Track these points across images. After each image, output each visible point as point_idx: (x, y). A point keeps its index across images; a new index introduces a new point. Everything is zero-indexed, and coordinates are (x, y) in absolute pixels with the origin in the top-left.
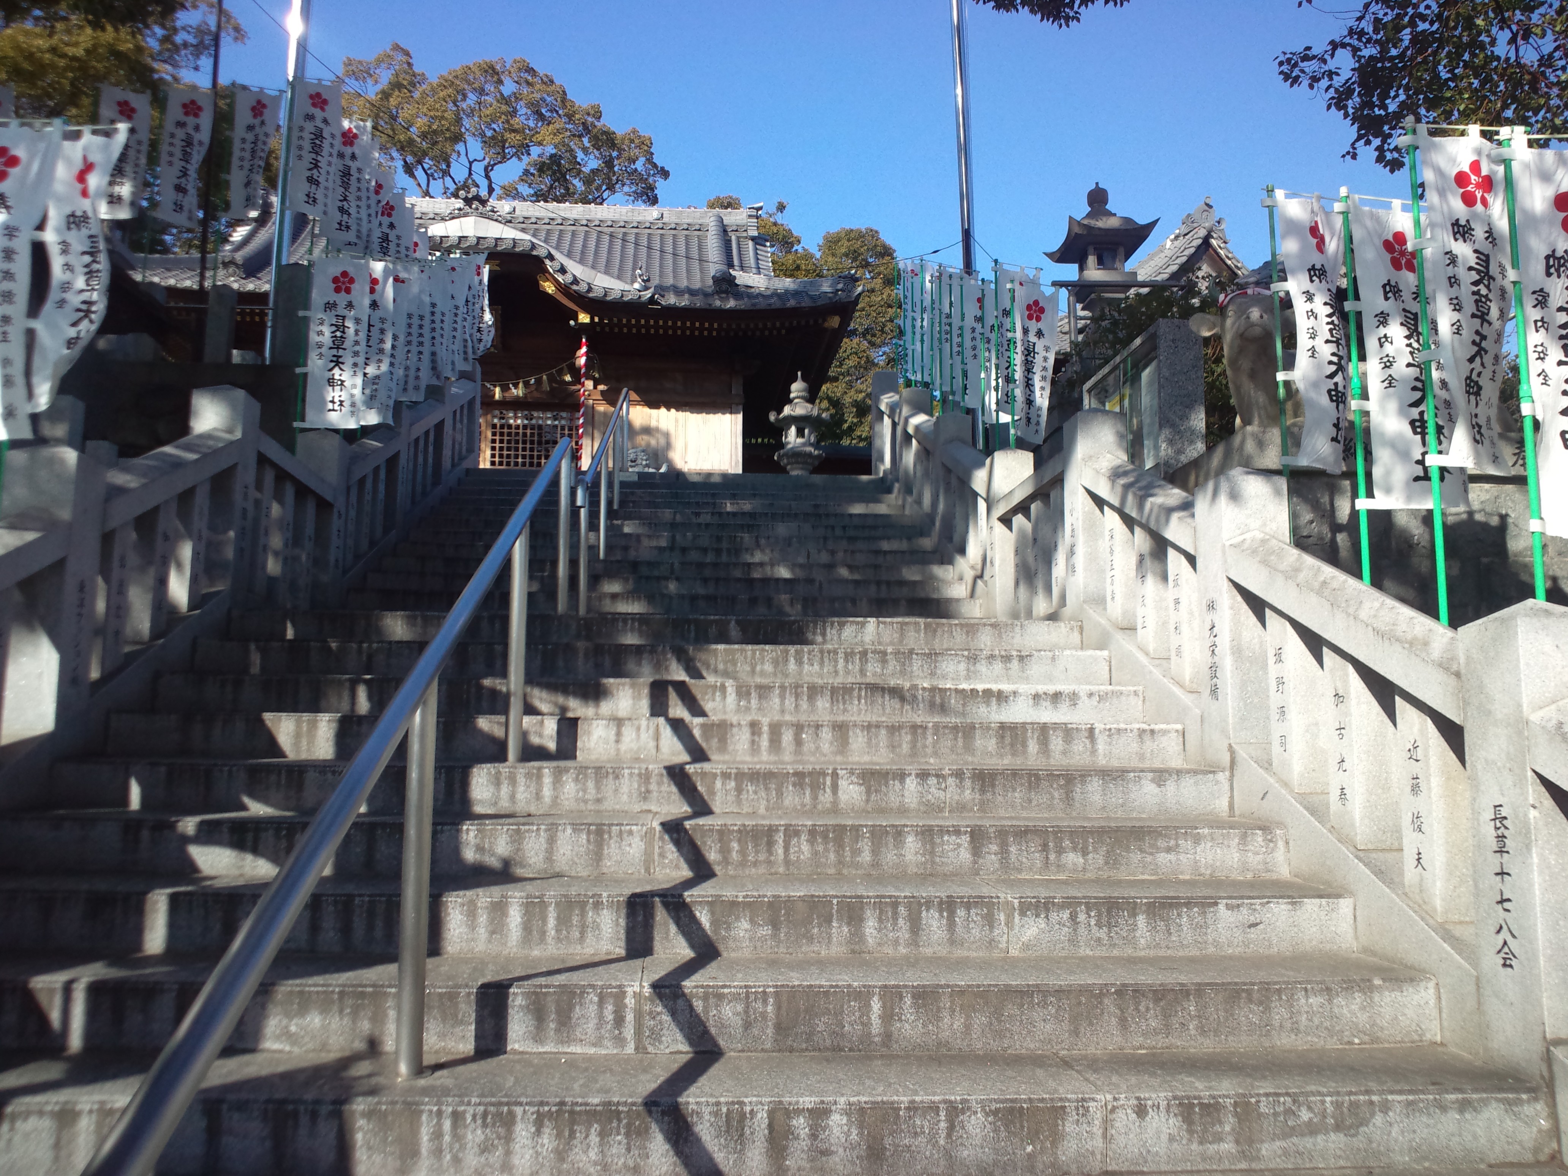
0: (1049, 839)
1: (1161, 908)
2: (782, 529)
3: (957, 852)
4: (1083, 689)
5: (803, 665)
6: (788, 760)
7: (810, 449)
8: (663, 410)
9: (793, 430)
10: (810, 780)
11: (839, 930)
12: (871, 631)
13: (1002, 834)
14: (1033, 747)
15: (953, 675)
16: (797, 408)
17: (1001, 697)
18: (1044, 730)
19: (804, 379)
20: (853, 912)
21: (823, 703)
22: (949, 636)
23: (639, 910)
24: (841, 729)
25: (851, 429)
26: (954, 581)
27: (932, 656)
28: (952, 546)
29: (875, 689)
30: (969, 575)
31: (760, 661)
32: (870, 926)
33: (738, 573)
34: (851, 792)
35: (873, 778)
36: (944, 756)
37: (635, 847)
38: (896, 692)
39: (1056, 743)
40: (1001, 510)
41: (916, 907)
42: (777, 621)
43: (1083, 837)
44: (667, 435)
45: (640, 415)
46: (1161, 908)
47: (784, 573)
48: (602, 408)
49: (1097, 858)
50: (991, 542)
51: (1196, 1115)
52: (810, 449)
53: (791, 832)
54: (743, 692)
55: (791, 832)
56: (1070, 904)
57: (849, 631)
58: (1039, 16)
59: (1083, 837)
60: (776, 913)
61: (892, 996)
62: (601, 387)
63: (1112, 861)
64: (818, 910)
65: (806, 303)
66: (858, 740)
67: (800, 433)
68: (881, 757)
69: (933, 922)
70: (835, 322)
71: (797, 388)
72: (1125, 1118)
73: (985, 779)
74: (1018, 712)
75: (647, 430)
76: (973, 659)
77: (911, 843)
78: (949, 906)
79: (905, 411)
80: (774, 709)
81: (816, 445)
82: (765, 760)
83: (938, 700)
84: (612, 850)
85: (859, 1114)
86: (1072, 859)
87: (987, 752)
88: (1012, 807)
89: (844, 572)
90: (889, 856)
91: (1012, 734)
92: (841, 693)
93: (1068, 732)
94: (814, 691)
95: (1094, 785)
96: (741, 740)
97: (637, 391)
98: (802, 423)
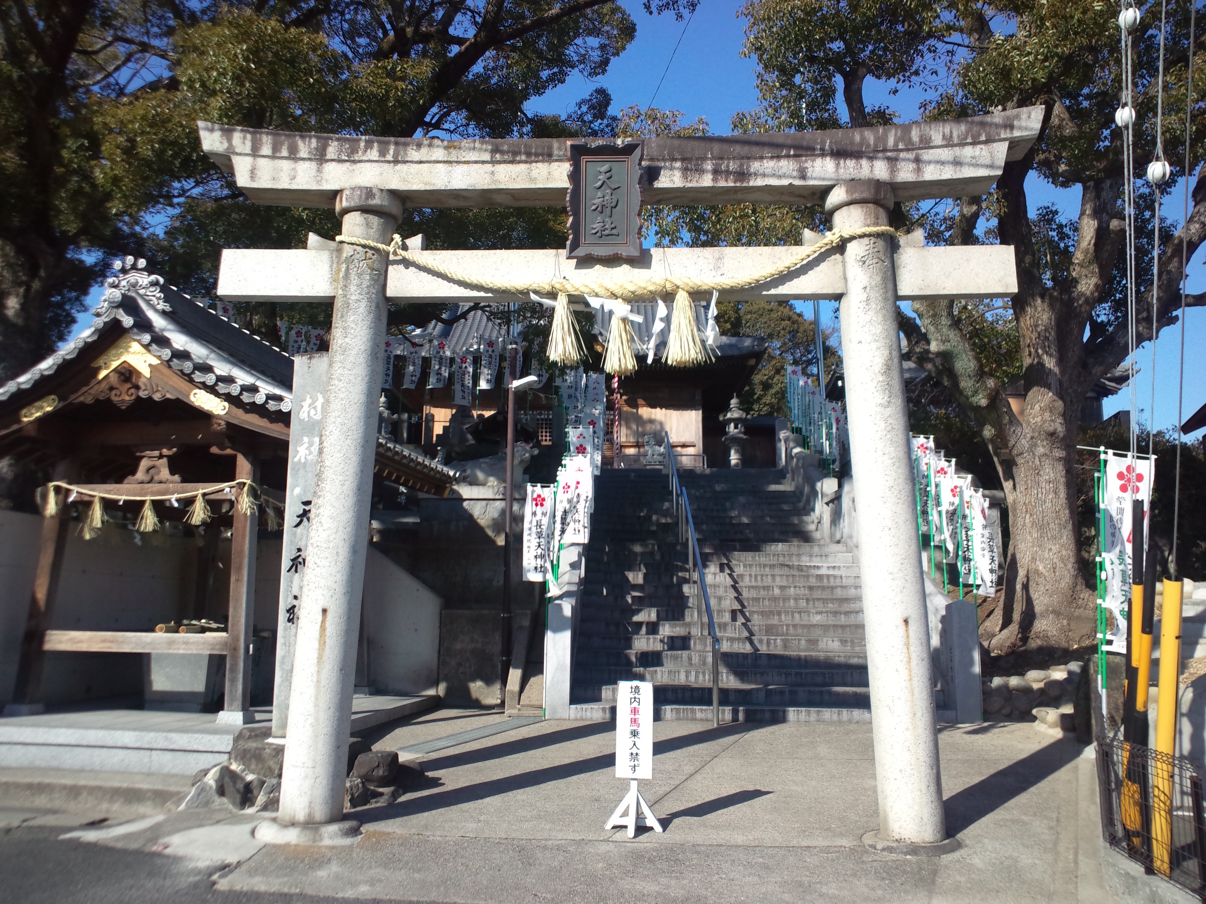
0: (824, 601)
1: (847, 613)
2: (742, 499)
3: (803, 603)
4: (842, 565)
5: (760, 558)
6: (759, 584)
7: (742, 435)
8: (658, 409)
9: (732, 425)
10: (767, 588)
11: (776, 617)
12: (780, 547)
13: (814, 600)
14: (825, 581)
15: (805, 561)
16: (734, 413)
17: (818, 567)
18: (828, 576)
19: (738, 397)
20: (779, 614)
21: (767, 569)
22: (806, 547)
23: (734, 613)
24: (773, 576)
25: (759, 398)
26: (810, 523)
27: (799, 555)
28: (809, 509)
29: (783, 565)
30: (816, 521)
31: (748, 557)
32: (783, 616)
33: (728, 520)
34: (777, 591)
35: (782, 588)
36: (801, 583)
37: (728, 602)
38: (788, 566)
39: (832, 580)
40: (826, 500)
41: (793, 612)
42: (752, 545)
43: (832, 600)
44: (661, 424)
45: (645, 412)
46: (847, 613)
47: (745, 520)
48: (626, 408)
49: (836, 605)
50: (821, 509)
51: (843, 642)
52: (742, 435)
53: (764, 599)
54: (745, 566)
55: (764, 599)
56: (827, 612)
57: (773, 547)
58: (884, 78)
59: (832, 600)
60: (762, 613)
61: (788, 626)
62: (624, 397)
63: (840, 606)
64: (772, 613)
65: (735, 353)
66: (778, 579)
67: (736, 427)
68: (784, 583)
69: (797, 616)
70: (752, 362)
71: (734, 402)
72: (830, 642)
73: (811, 588)
74: (823, 571)
75: (651, 421)
76: (811, 556)
77: (792, 601)
78: (800, 613)
79: (792, 444)
80: (754, 571)
81: (745, 433)
82: (754, 583)
83: (800, 568)
84: (723, 602)
85: (782, 640)
86: (830, 605)
87: (813, 582)
88: (817, 594)
89: (768, 519)
90: (787, 604)
91: (820, 577)
92: (772, 566)
93: (835, 577)
94: (765, 566)
95: (839, 589)
96: (747, 579)
97: (644, 399)
98: (737, 421)
